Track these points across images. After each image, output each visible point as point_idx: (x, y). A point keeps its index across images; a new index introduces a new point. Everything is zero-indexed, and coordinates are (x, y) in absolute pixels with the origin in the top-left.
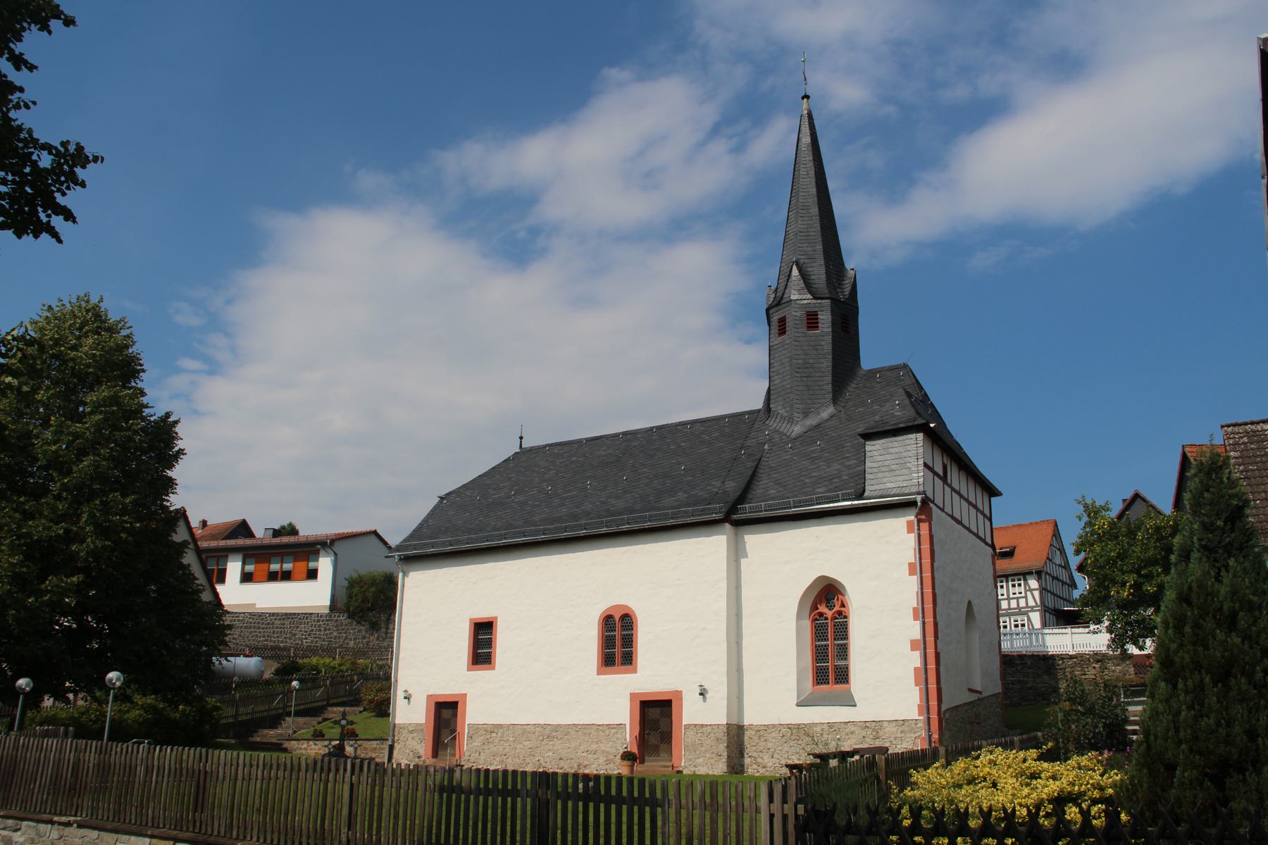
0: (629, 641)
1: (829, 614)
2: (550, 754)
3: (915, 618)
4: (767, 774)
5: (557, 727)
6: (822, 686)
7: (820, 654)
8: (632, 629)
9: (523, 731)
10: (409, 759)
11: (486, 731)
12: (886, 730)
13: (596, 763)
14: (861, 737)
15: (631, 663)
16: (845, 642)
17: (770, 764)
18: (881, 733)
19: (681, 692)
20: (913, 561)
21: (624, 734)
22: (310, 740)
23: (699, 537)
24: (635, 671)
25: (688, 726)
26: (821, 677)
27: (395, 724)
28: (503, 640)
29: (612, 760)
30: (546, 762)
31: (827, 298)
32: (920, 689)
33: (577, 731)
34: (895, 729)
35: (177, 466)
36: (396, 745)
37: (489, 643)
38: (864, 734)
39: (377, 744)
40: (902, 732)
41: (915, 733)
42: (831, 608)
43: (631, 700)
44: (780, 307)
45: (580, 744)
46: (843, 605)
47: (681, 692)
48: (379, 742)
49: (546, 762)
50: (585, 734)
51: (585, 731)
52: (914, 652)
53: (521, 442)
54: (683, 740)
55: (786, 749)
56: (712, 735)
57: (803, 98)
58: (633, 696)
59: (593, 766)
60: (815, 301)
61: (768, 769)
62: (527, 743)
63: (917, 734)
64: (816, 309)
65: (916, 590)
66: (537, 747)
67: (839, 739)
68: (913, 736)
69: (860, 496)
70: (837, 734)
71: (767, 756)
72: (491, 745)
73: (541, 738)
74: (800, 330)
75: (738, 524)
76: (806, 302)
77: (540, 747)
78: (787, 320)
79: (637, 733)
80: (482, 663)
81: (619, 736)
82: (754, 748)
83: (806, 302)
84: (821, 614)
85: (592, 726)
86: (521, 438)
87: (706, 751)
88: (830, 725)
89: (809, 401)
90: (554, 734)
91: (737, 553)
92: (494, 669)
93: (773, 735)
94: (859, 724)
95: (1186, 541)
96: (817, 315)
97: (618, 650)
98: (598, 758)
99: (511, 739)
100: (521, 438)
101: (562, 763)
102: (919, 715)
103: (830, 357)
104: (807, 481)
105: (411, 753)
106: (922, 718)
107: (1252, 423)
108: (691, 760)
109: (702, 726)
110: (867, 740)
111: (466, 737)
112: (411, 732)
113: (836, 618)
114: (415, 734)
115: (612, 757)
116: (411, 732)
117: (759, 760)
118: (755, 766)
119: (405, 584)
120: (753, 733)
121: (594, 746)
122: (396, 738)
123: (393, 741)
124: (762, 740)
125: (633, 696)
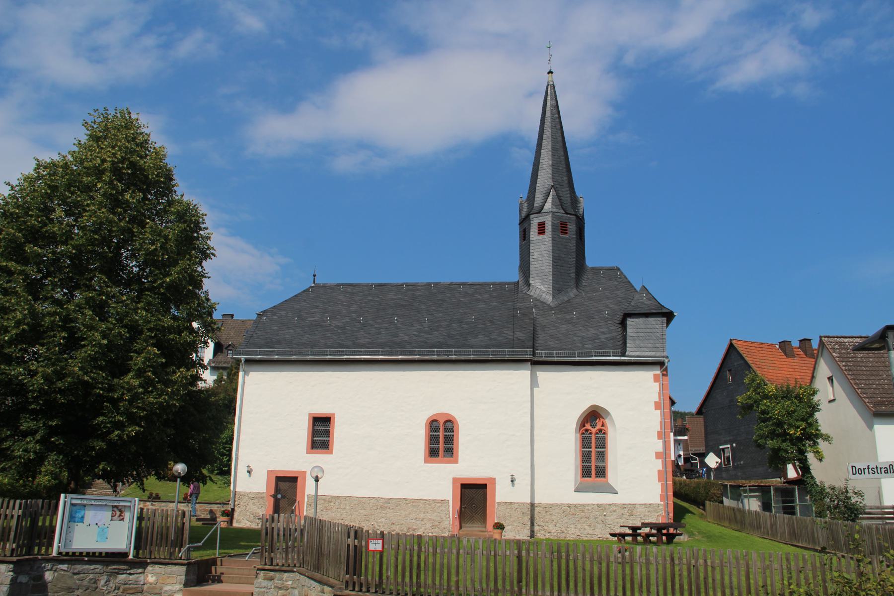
0: (433, 439)
1: (594, 430)
2: (383, 520)
4: (552, 538)
5: (388, 501)
6: (586, 479)
7: (585, 457)
8: (453, 431)
9: (360, 502)
10: (250, 520)
11: (324, 500)
12: (638, 510)
13: (423, 528)
15: (604, 477)
16: (603, 450)
17: (553, 531)
18: (634, 511)
19: (495, 479)
20: (657, 400)
21: (447, 507)
22: (146, 501)
24: (456, 462)
25: (499, 503)
26: (586, 472)
27: (235, 493)
28: (339, 433)
29: (437, 525)
30: (380, 526)
31: (573, 215)
32: (662, 484)
34: (644, 510)
36: (236, 508)
37: (327, 433)
38: (622, 511)
39: (218, 507)
40: (649, 512)
42: (594, 427)
44: (540, 215)
45: (410, 514)
46: (603, 425)
47: (495, 479)
48: (220, 505)
49: (380, 526)
50: (414, 506)
52: (307, 417)
53: (314, 278)
54: (495, 515)
55: (566, 521)
56: (519, 510)
57: (549, 73)
58: (455, 480)
59: (421, 530)
60: (566, 215)
61: (552, 534)
62: (362, 511)
63: (659, 513)
64: (567, 221)
65: (660, 419)
66: (372, 515)
67: (605, 515)
68: (657, 514)
69: (623, 355)
70: (604, 512)
71: (552, 525)
72: (329, 512)
73: (375, 508)
74: (557, 233)
75: (535, 363)
76: (558, 214)
78: (546, 225)
79: (458, 507)
80: (317, 448)
81: (444, 508)
82: (542, 519)
83: (560, 214)
84: (587, 430)
85: (421, 501)
86: (315, 276)
87: (514, 521)
88: (599, 505)
89: (562, 283)
90: (386, 505)
91: (534, 383)
92: (332, 453)
96: (544, 224)
97: (441, 446)
98: (425, 524)
99: (348, 508)
100: (315, 276)
101: (394, 527)
103: (575, 255)
104: (575, 338)
105: (252, 515)
106: (662, 503)
107: (837, 337)
110: (625, 516)
111: (305, 504)
112: (252, 499)
113: (597, 433)
114: (256, 501)
115: (437, 523)
116: (252, 499)
117: (546, 528)
118: (542, 532)
119: (246, 381)
120: (541, 509)
121: (422, 515)
122: (236, 503)
123: (234, 506)
125: (455, 480)
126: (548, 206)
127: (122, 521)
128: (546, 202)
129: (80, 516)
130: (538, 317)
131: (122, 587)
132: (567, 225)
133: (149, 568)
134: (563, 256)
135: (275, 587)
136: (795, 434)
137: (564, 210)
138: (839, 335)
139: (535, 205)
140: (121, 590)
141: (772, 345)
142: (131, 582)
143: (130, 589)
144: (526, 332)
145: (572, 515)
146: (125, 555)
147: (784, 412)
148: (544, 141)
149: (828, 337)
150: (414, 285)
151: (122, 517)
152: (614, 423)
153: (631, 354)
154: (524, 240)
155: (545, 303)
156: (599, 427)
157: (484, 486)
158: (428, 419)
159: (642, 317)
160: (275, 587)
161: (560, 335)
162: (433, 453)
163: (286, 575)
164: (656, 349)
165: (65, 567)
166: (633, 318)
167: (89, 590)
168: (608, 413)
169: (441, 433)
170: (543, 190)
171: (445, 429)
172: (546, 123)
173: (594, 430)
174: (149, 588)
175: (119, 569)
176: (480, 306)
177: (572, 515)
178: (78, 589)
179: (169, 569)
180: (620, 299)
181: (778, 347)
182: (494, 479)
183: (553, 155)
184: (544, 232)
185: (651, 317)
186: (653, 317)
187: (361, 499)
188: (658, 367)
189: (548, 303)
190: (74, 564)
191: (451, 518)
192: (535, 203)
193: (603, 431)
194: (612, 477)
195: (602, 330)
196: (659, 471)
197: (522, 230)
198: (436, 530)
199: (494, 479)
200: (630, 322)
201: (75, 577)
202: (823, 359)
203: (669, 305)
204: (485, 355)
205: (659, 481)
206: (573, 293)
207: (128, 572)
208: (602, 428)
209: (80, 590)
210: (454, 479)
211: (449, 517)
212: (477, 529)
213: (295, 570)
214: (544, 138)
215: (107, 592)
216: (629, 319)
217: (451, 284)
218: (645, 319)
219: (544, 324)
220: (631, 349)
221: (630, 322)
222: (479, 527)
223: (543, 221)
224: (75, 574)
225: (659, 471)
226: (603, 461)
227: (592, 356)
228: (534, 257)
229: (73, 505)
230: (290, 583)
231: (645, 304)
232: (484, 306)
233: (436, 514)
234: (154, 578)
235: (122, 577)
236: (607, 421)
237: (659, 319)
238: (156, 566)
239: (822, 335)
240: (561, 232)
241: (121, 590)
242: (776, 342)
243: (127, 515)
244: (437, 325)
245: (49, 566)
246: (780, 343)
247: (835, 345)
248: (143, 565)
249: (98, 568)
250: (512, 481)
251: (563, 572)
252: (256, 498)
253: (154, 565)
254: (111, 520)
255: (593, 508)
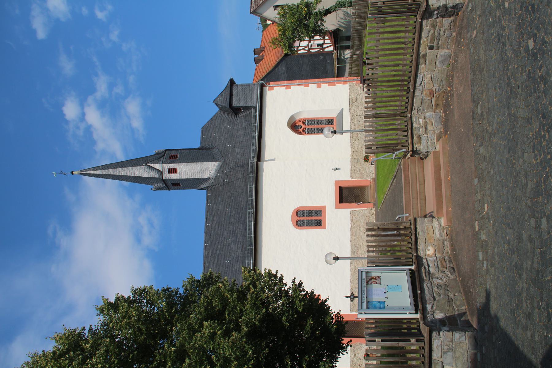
0: (309, 224)
3: (309, 86)
8: (304, 211)
14: (356, 107)
16: (316, 121)
18: (354, 99)
21: (355, 212)
23: (263, 175)
25: (352, 177)
33: (354, 239)
35: (186, 280)
38: (354, 106)
41: (354, 86)
43: (339, 208)
44: (163, 172)
51: (354, 235)
52: (323, 205)
58: (337, 207)
63: (355, 85)
65: (297, 86)
67: (357, 116)
69: (256, 108)
70: (355, 117)
75: (259, 159)
76: (164, 160)
77: (363, 262)
78: (170, 168)
83: (164, 159)
84: (303, 131)
87: (363, 168)
88: (351, 120)
93: (355, 145)
94: (351, 107)
95: (279, 308)
96: (170, 169)
97: (314, 218)
102: (347, 84)
106: (348, 83)
107: (251, 5)
108: (367, 175)
109: (351, 170)
110: (357, 104)
112: (355, 355)
113: (305, 125)
114: (356, 352)
115: (367, 218)
116: (355, 355)
120: (354, 154)
124: (357, 150)
125: (337, 207)
126: (157, 166)
127: (381, 278)
128: (154, 168)
129: (379, 304)
130: (230, 168)
131: (441, 269)
132: (171, 156)
133: (421, 254)
134: (191, 157)
135: (426, 133)
136: (306, 11)
137: (162, 157)
138: (250, 4)
139: (157, 177)
140: (444, 269)
141: (256, 68)
142: (436, 265)
143: (442, 264)
144: (238, 172)
145: (357, 135)
146: (412, 272)
147: (292, 17)
148: (116, 174)
149: (251, 9)
150: (205, 258)
151: (377, 278)
152: (298, 112)
153: (255, 103)
154: (179, 185)
155: (221, 166)
156: (301, 124)
157: (341, 189)
158: (295, 227)
159: (233, 98)
160: (426, 133)
161: (242, 151)
162: (319, 224)
163: (415, 125)
164: (253, 89)
165: (429, 307)
166: (233, 103)
167: (448, 289)
168: (292, 117)
169: (305, 218)
170: (147, 172)
171: (302, 216)
172: (105, 174)
173: (303, 126)
174: (439, 252)
175: (425, 272)
176: (221, 208)
177: (357, 135)
178: (449, 296)
179: (420, 235)
180: (221, 121)
181: (258, 65)
182: (336, 181)
183: (126, 167)
184: (175, 169)
185: (233, 93)
186: (233, 91)
187: (352, 272)
188: (264, 88)
189: (221, 163)
190: (426, 301)
191: (362, 209)
192: (155, 177)
193: (304, 121)
194: (333, 115)
195: (240, 126)
196: (328, 86)
197: (173, 188)
198: (371, 219)
199: (336, 181)
200: (235, 104)
201: (437, 299)
202: (264, 12)
203: (226, 82)
204: (252, 190)
205: (335, 85)
206: (215, 151)
207: (427, 267)
208: (302, 121)
209: (449, 295)
210: (336, 208)
211: (362, 210)
212: (369, 192)
213: (409, 115)
214: (114, 174)
215: (447, 278)
216: (233, 105)
217: (206, 233)
218: (233, 96)
219: (234, 163)
220: (252, 103)
221: (235, 104)
222: (368, 191)
223: (167, 170)
224: (434, 300)
225: (328, 86)
226: (323, 121)
227: (256, 126)
228: (191, 175)
229: (368, 308)
230: (421, 120)
231: (224, 97)
232: (221, 206)
233: (360, 219)
234: (430, 248)
235: (432, 270)
236: (298, 118)
237: (234, 88)
238: (419, 247)
239: (250, 12)
240: (176, 158)
241: (444, 269)
242: (255, 65)
243: (374, 275)
244: (231, 232)
245: (429, 317)
246: (255, 63)
247: (255, 5)
248: (419, 260)
249: (427, 285)
250: (337, 169)
251: (392, 52)
252: (354, 351)
253: (418, 250)
254: (380, 284)
255: (353, 123)
